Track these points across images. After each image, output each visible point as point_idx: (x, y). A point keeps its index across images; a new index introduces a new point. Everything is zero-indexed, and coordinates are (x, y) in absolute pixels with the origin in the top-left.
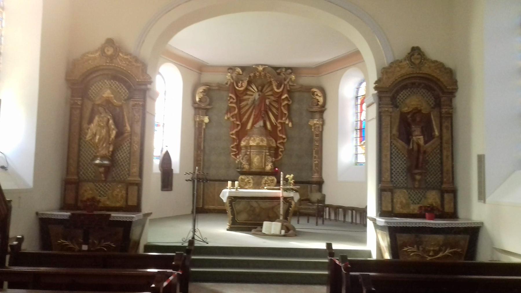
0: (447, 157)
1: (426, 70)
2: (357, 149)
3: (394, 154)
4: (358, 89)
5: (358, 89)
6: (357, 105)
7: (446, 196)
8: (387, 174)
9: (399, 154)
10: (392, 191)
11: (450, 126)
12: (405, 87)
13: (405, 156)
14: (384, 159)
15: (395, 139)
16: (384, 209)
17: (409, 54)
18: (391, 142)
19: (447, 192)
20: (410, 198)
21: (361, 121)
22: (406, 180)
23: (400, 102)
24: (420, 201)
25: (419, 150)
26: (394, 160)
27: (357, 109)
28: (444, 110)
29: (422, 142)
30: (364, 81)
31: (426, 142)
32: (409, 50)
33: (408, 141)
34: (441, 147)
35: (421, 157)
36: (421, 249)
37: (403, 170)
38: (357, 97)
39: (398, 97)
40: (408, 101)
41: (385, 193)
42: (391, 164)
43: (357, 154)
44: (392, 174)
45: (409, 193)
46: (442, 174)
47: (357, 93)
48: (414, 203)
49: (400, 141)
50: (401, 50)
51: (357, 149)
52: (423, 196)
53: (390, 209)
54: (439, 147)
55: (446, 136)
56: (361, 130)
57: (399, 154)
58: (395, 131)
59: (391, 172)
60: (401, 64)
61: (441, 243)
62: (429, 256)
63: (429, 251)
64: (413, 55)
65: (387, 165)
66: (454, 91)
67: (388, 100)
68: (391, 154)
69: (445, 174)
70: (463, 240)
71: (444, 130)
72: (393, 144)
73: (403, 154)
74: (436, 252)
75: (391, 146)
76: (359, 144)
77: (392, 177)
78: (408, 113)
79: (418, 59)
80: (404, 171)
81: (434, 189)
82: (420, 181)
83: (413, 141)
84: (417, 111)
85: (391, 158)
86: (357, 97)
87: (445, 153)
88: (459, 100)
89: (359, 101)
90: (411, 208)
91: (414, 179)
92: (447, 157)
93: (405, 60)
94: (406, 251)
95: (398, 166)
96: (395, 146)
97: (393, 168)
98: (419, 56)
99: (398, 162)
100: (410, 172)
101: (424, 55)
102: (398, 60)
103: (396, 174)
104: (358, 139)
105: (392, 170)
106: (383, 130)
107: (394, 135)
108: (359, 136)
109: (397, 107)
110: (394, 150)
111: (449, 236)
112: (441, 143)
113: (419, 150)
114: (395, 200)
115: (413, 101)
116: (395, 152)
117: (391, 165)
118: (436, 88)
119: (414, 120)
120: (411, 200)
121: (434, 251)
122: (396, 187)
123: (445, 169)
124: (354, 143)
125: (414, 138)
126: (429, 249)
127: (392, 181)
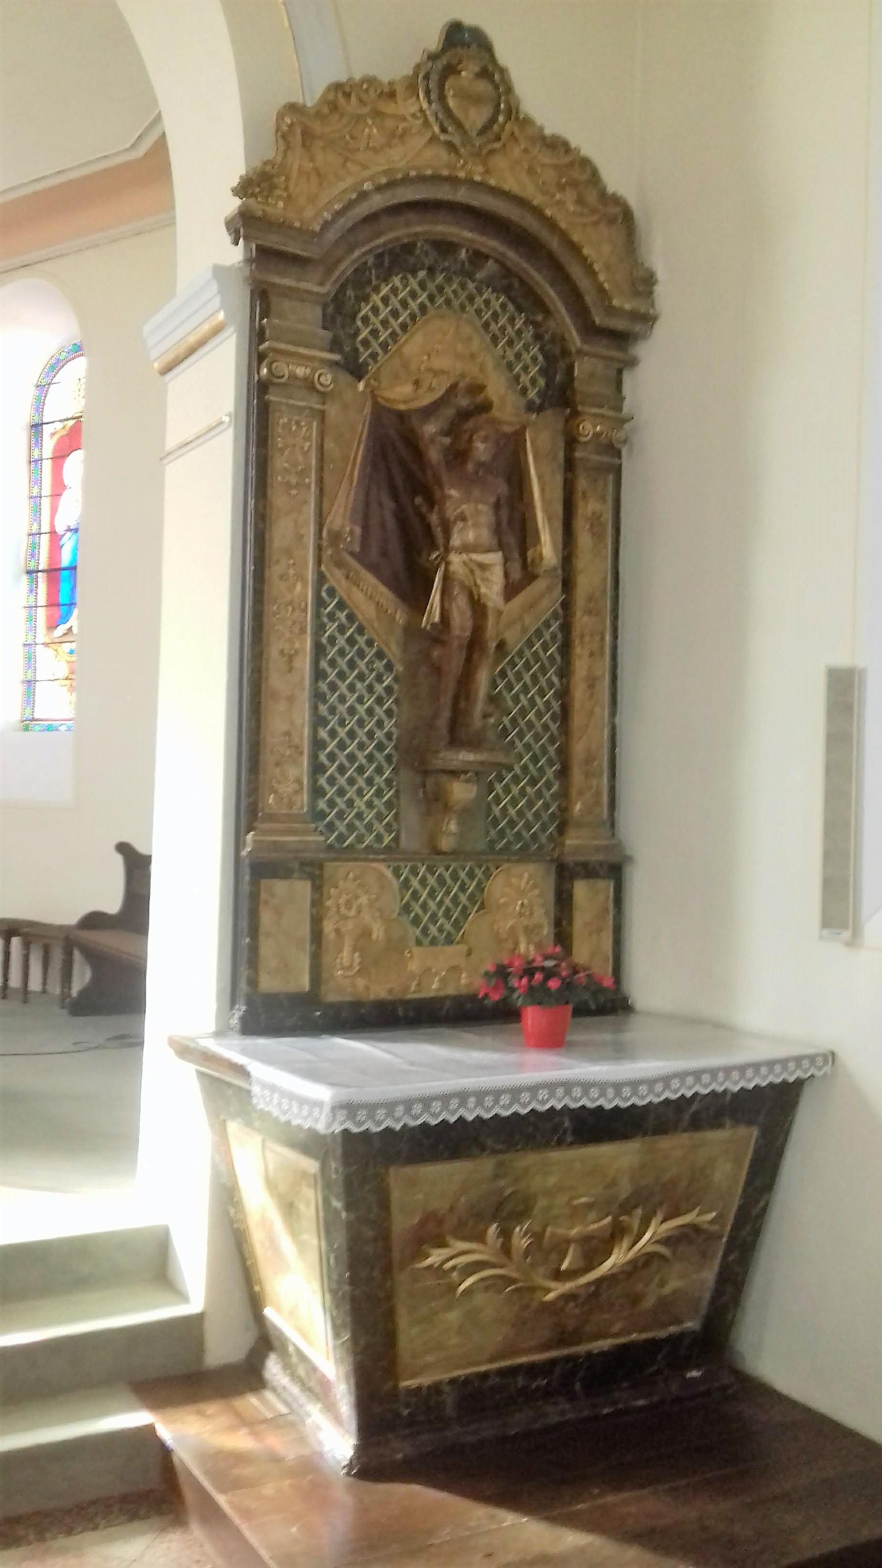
0: (592, 683)
1: (510, 174)
2: (30, 661)
3: (332, 652)
4: (43, 388)
5: (43, 388)
6: (34, 462)
7: (581, 890)
8: (292, 772)
9: (361, 654)
10: (314, 871)
11: (608, 516)
12: (397, 260)
13: (389, 667)
14: (276, 680)
15: (339, 564)
16: (268, 984)
17: (433, 57)
18: (321, 579)
19: (589, 871)
20: (406, 909)
21: (55, 537)
22: (389, 805)
23: (375, 346)
24: (457, 925)
25: (475, 643)
26: (333, 687)
27: (35, 480)
28: (588, 429)
29: (492, 589)
30: (77, 350)
31: (511, 591)
32: (433, 41)
33: (412, 583)
34: (566, 628)
35: (483, 678)
36: (520, 1241)
37: (380, 747)
38: (37, 427)
39: (365, 310)
40: (414, 345)
41: (280, 887)
42: (315, 709)
43: (30, 684)
44: (317, 769)
45: (406, 885)
46: (564, 773)
47: (39, 406)
48: (426, 939)
49: (370, 579)
50: (389, 38)
51: (30, 661)
52: (472, 898)
53: (304, 983)
54: (555, 626)
55: (590, 576)
56: (54, 572)
57: (361, 654)
58: (341, 516)
59: (314, 757)
60: (389, 108)
61: (625, 1189)
62: (558, 1275)
63: (560, 1247)
64: (451, 70)
65: (291, 717)
66: (637, 328)
67: (305, 318)
68: (319, 650)
69: (577, 776)
70: (724, 1154)
71: (584, 539)
72: (332, 592)
73: (380, 655)
74: (595, 1249)
75: (320, 603)
76: (42, 635)
77: (317, 792)
78: (429, 412)
79: (476, 100)
80: (380, 757)
81: (524, 856)
82: (465, 813)
83: (447, 578)
84: (467, 409)
85: (319, 675)
86: (37, 427)
87: (581, 666)
88: (660, 383)
89: (49, 446)
90: (414, 966)
91: (435, 802)
92: (592, 683)
93: (412, 87)
94: (437, 1271)
95: (351, 723)
96: (341, 605)
97: (323, 734)
98: (483, 87)
99: (351, 699)
100: (417, 761)
101: (509, 90)
102: (371, 81)
103: (342, 770)
104: (42, 614)
105: (318, 744)
106: (279, 499)
107: (336, 537)
108: (42, 599)
109: (357, 371)
110: (332, 628)
111: (665, 1143)
112: (567, 605)
113: (475, 643)
114: (328, 927)
115: (440, 349)
116: (341, 641)
117: (318, 721)
118: (551, 294)
119: (458, 456)
120: (416, 921)
121: (585, 1240)
122: (342, 852)
123: (579, 748)
124: (20, 635)
125: (456, 559)
126: (561, 1231)
127: (322, 815)
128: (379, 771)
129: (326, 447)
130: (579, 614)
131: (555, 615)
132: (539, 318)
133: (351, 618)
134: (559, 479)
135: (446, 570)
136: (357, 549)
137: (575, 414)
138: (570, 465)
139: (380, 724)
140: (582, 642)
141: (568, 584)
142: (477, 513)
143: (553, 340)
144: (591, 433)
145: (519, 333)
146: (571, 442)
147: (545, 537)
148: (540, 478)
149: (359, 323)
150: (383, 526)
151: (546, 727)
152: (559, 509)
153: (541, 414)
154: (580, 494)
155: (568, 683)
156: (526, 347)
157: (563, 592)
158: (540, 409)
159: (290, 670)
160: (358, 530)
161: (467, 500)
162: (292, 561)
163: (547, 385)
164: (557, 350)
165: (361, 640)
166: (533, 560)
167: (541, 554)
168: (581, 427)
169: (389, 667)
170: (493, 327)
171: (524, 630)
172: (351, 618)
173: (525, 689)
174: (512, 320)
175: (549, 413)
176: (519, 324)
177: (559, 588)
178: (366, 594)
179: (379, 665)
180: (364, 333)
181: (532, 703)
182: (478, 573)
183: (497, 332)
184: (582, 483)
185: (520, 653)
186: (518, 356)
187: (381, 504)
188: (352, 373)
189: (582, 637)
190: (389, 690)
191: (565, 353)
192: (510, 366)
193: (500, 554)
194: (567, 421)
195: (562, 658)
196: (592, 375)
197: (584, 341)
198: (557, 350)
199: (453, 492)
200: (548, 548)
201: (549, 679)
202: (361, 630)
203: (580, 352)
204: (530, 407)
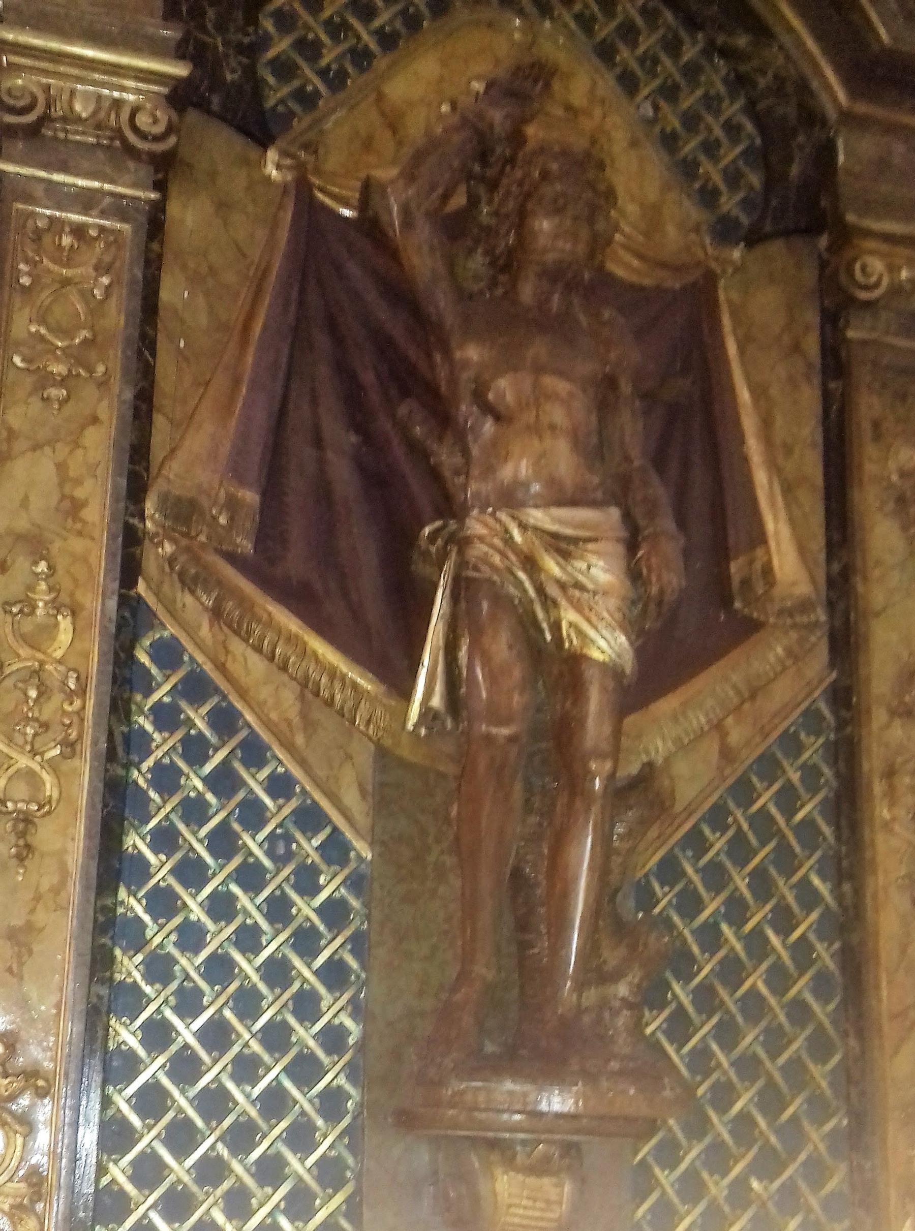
3: (163, 810)
9: (253, 816)
34: (846, 752)
54: (813, 749)
72: (169, 654)
73: (309, 818)
107: (183, 513)
112: (845, 697)
128: (301, 1138)
129: (165, 295)
130: (879, 716)
131: (812, 720)
132: (742, 41)
133: (225, 721)
134: (809, 397)
135: (462, 564)
136: (245, 545)
137: (844, 236)
138: (835, 363)
139: (306, 1007)
140: (891, 795)
141: (845, 642)
142: (540, 396)
143: (779, 87)
144: (885, 281)
145: (692, 72)
146: (837, 303)
147: (776, 526)
148: (759, 392)
149: (268, 25)
150: (324, 493)
151: (799, 1012)
152: (811, 464)
153: (759, 250)
154: (866, 426)
155: (858, 892)
156: (711, 102)
157: (832, 665)
158: (754, 238)
159: (26, 853)
160: (250, 497)
161: (509, 362)
162: (42, 567)
163: (769, 185)
164: (789, 110)
165: (255, 783)
166: (746, 583)
167: (768, 571)
168: (858, 266)
169: (337, 850)
170: (624, 53)
171: (727, 754)
172: (225, 721)
173: (736, 911)
174: (673, 47)
175: (776, 247)
176: (690, 53)
177: (822, 653)
178: (271, 658)
179: (309, 847)
180: (281, 46)
181: (757, 944)
182: (551, 566)
183: (634, 65)
184: (869, 405)
185: (718, 817)
186: (691, 121)
187: (318, 442)
188: (244, 130)
189: (890, 773)
190: (334, 913)
191: (811, 117)
192: (669, 141)
193: (615, 513)
194: (823, 265)
195: (838, 828)
196: (882, 165)
197: (853, 93)
198: (789, 110)
199: (472, 353)
200: (787, 554)
201: (805, 882)
202: (254, 754)
203: (847, 117)
204: (725, 231)
